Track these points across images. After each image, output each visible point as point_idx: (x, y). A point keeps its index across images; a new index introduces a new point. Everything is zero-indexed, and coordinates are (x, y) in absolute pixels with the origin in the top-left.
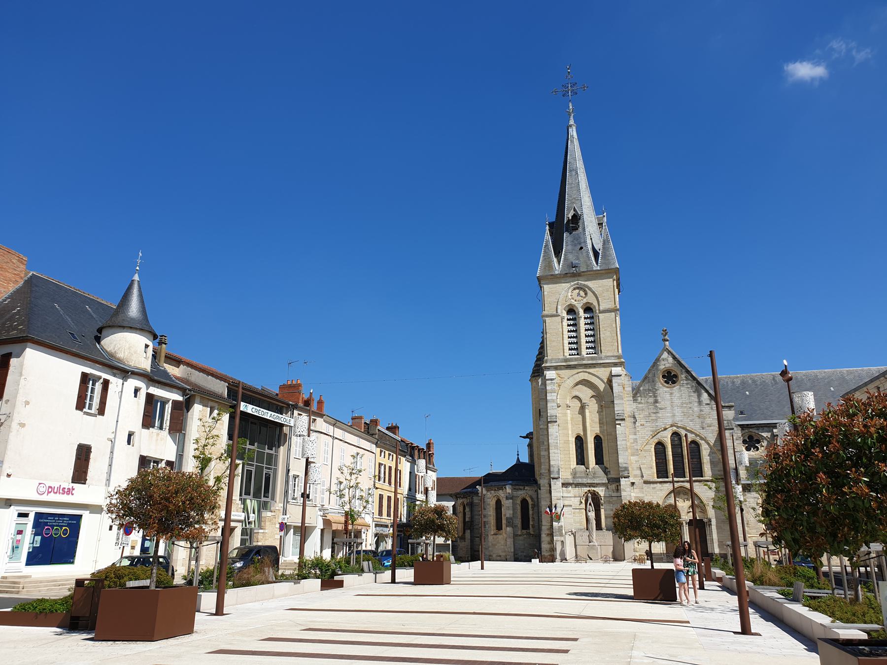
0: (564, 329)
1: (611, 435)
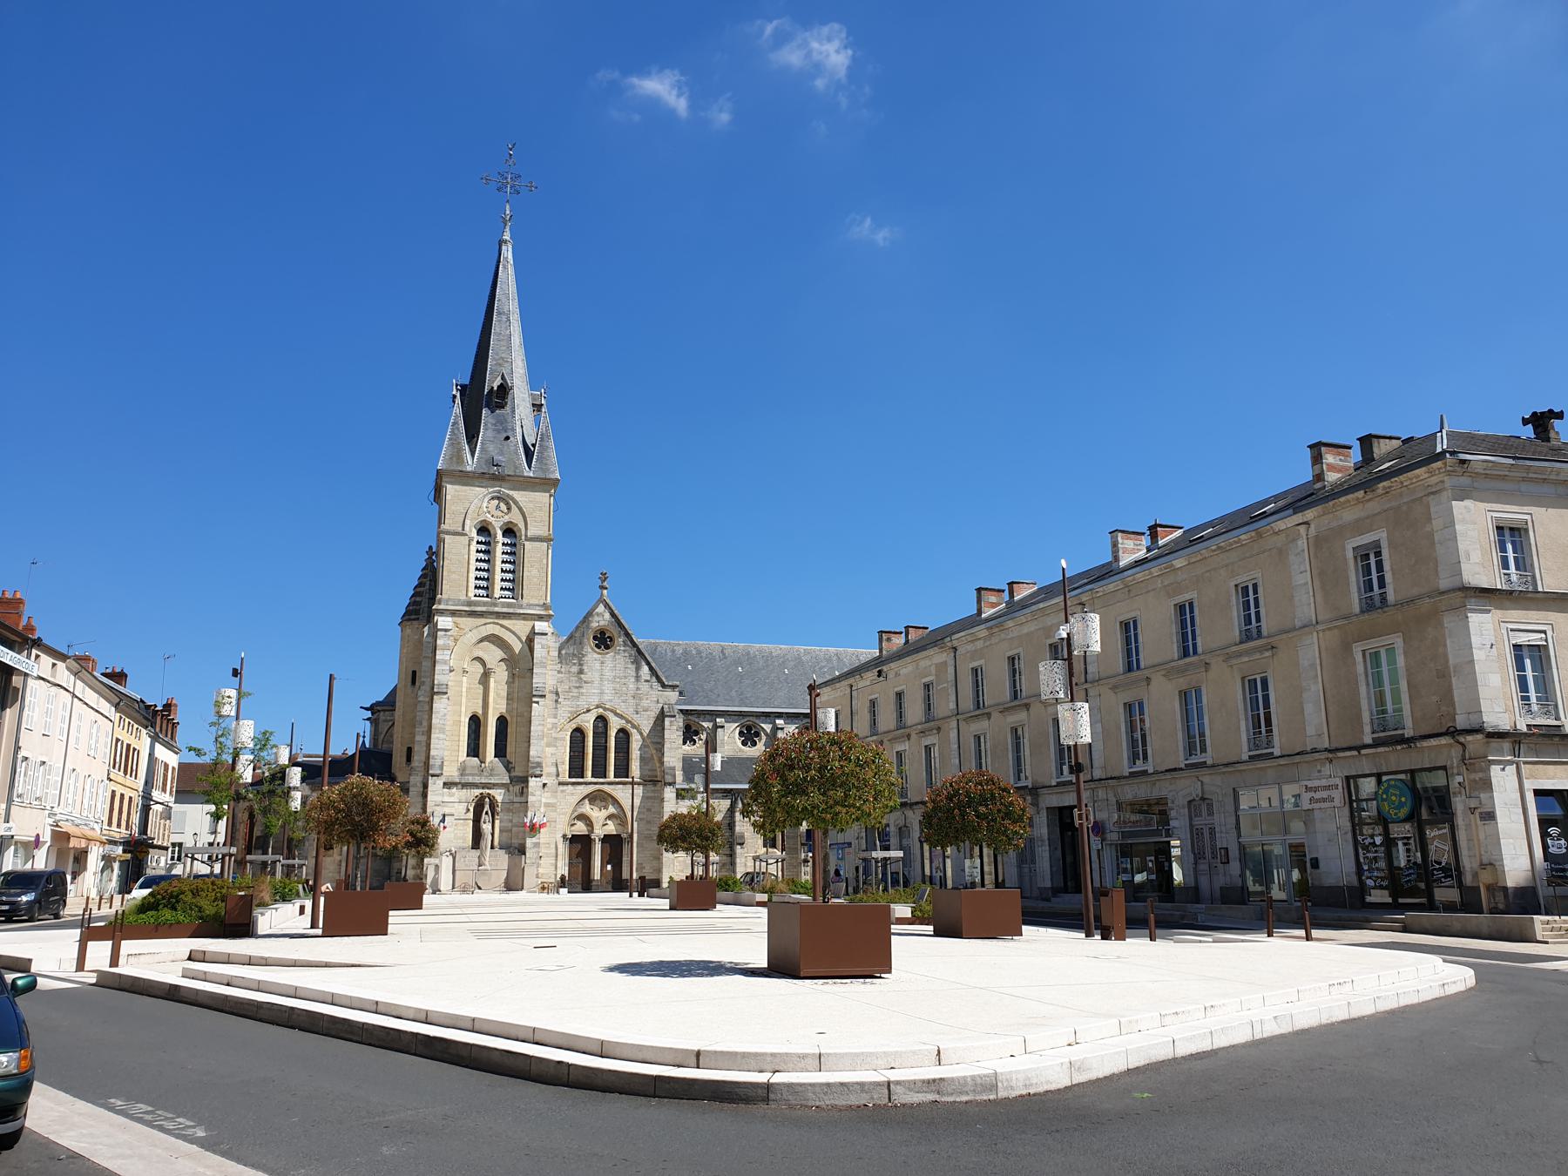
0: (471, 557)
1: (522, 716)
